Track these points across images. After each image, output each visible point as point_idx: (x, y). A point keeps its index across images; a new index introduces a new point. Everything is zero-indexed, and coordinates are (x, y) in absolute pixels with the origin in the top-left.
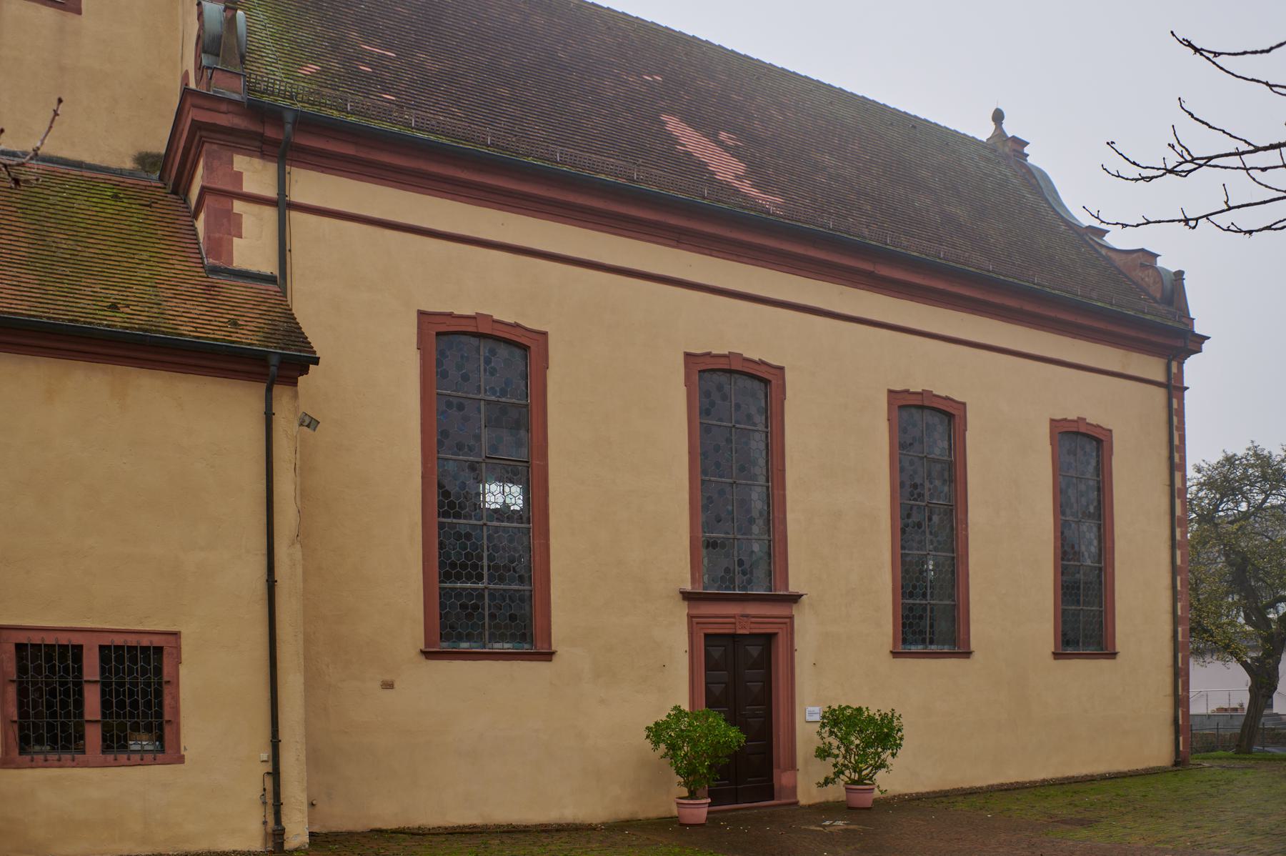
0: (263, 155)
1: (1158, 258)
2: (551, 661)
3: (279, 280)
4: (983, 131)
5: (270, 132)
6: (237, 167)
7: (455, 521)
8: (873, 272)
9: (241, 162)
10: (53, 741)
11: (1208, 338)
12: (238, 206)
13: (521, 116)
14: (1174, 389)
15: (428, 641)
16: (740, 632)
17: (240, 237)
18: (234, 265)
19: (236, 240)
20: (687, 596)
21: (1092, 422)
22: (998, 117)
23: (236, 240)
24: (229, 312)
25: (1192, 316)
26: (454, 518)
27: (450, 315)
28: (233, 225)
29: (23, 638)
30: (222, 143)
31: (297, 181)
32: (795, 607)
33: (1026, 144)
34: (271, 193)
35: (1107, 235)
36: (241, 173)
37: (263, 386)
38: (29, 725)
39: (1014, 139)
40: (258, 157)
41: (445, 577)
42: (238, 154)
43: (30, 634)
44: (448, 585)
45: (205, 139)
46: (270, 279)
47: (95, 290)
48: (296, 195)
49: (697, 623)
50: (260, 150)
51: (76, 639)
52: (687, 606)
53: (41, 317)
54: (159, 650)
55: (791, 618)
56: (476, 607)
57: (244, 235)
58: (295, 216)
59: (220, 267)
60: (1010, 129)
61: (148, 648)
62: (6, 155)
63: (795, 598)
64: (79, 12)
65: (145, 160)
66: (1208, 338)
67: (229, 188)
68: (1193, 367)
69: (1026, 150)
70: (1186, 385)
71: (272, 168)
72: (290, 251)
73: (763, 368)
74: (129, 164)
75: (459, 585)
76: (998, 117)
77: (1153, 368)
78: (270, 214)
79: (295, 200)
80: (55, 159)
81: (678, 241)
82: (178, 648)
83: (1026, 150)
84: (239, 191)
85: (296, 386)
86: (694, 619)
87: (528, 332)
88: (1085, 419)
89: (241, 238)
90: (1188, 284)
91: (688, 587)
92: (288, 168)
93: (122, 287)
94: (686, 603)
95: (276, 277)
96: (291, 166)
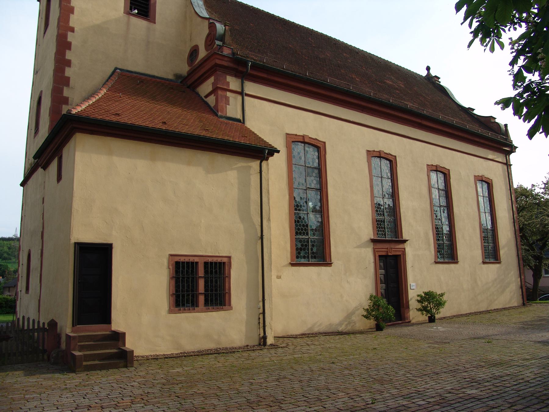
0: (236, 76)
1: (496, 119)
2: (331, 266)
3: (242, 121)
4: (424, 73)
5: (241, 69)
7: (299, 212)
8: (421, 123)
9: (229, 79)
11: (518, 147)
12: (229, 94)
14: (508, 165)
15: (292, 260)
16: (390, 254)
20: (373, 241)
21: (486, 177)
22: (428, 69)
25: (512, 140)
26: (299, 211)
27: (296, 135)
29: (207, 259)
31: (246, 86)
32: (405, 244)
33: (439, 78)
34: (239, 90)
35: (474, 110)
36: (229, 82)
37: (258, 162)
38: (213, 294)
39: (436, 76)
40: (234, 77)
41: (297, 233)
43: (180, 258)
44: (297, 237)
45: (217, 70)
46: (238, 120)
47: (132, 121)
48: (247, 91)
49: (377, 251)
51: (196, 259)
52: (373, 244)
53: (206, 136)
54: (177, 263)
55: (405, 249)
56: (306, 246)
58: (246, 98)
60: (433, 73)
61: (189, 262)
62: (130, 72)
63: (405, 241)
64: (155, 23)
65: (178, 76)
66: (518, 147)
67: (225, 87)
68: (512, 156)
69: (440, 80)
70: (511, 164)
71: (239, 81)
73: (390, 156)
74: (171, 77)
75: (301, 237)
76: (428, 69)
77: (500, 158)
78: (239, 98)
80: (183, 75)
81: (362, 111)
82: (230, 263)
83: (440, 80)
84: (228, 88)
86: (376, 250)
87: (314, 140)
88: (484, 176)
90: (509, 128)
91: (372, 238)
94: (372, 243)
96: (245, 80)
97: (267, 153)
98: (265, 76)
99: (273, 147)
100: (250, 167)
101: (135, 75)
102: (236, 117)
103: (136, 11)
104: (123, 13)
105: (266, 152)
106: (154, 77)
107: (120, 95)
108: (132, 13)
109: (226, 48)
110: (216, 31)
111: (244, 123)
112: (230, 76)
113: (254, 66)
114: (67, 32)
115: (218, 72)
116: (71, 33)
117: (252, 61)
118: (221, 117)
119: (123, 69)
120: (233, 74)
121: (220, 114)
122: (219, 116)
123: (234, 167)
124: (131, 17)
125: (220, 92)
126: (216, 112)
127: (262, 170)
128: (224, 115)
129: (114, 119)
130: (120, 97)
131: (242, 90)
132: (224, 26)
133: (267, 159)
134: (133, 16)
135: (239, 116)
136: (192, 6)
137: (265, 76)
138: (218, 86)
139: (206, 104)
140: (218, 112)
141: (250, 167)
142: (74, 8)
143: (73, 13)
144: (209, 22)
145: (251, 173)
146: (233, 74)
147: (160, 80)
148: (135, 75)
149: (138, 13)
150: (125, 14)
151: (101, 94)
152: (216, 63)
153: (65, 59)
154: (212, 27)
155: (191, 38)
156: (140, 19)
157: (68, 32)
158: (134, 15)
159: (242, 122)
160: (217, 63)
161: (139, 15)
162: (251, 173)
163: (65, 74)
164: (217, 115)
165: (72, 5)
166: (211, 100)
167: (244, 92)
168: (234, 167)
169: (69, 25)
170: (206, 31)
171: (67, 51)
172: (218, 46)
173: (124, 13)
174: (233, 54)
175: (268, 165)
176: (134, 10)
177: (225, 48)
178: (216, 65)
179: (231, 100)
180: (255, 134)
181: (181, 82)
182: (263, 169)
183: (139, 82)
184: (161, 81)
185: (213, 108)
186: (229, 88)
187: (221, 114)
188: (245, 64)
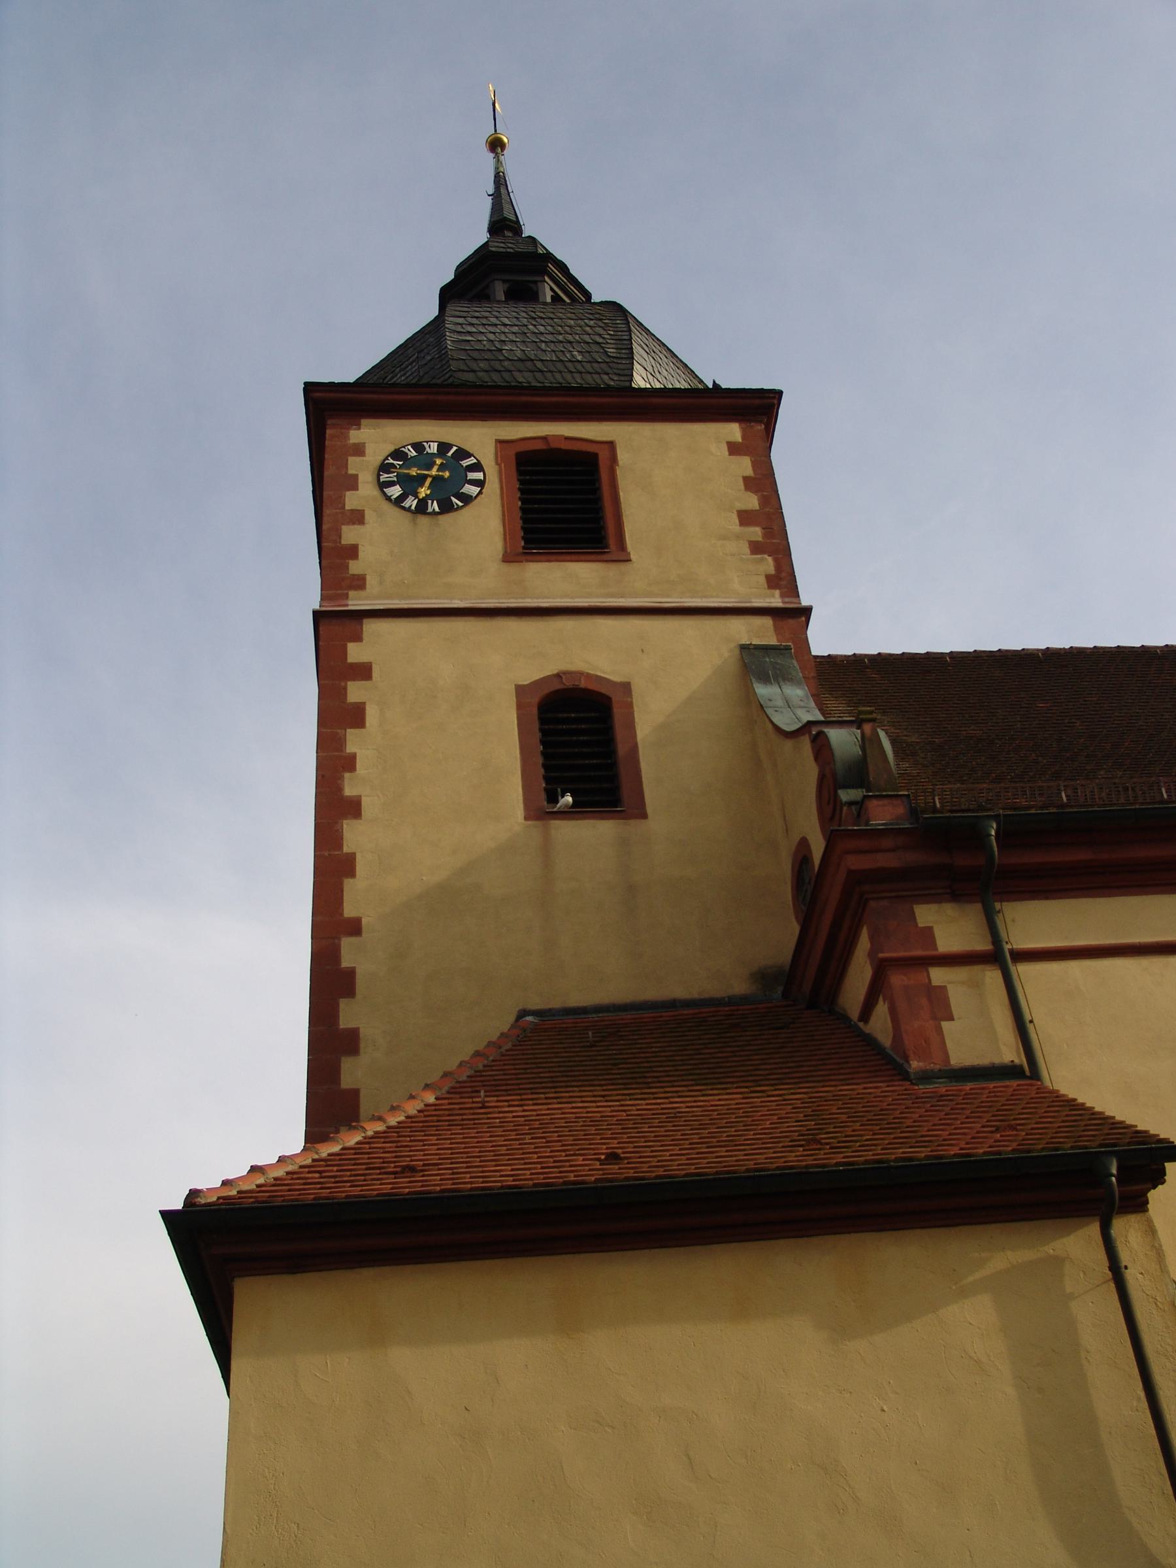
6: (922, 922)
9: (926, 915)
10: (341, 497)
12: (938, 975)
13: (441, 1123)
17: (951, 1018)
18: (952, 1062)
19: (945, 1025)
23: (945, 1025)
24: (579, 1054)
28: (939, 1006)
30: (893, 894)
34: (982, 945)
37: (1093, 1229)
42: (918, 903)
50: (948, 891)
57: (955, 1017)
58: (1025, 972)
59: (932, 1070)
64: (644, 816)
70: (805, 601)
71: (974, 911)
72: (1031, 1021)
74: (740, 987)
78: (992, 977)
79: (1019, 947)
85: (1146, 1210)
89: (953, 1020)
92: (997, 906)
93: (584, 1056)
95: (1021, 1067)
96: (1001, 901)
97: (1114, 1171)
98: (1082, 855)
99: (1142, 1137)
100: (1058, 1262)
101: (594, 1017)
102: (997, 1061)
103: (569, 799)
104: (523, 821)
105: (1108, 1169)
106: (672, 1004)
107: (480, 1100)
108: (555, 810)
109: (880, 803)
110: (833, 754)
111: (1035, 1074)
112: (927, 902)
113: (1009, 836)
114: (336, 941)
115: (872, 904)
116: (353, 939)
117: (999, 815)
118: (926, 1077)
119: (550, 1010)
120: (940, 891)
121: (915, 1065)
122: (912, 1076)
123: (970, 1279)
124: (556, 823)
125: (897, 980)
126: (901, 1061)
127: (1123, 1264)
128: (938, 1067)
129: (406, 1186)
130: (481, 1108)
131: (994, 943)
132: (858, 729)
133: (1138, 1205)
134: (559, 819)
135: (1009, 1053)
136: (764, 715)
137: (1082, 855)
138: (881, 955)
139: (870, 1041)
140: (908, 1062)
141: (1058, 1262)
142: (355, 859)
143: (351, 873)
144: (810, 736)
145: (1068, 1290)
146: (940, 891)
147: (691, 1012)
148: (594, 1017)
149: (575, 804)
150: (530, 822)
151: (404, 1112)
152: (850, 872)
153: (1147, 1193)
154: (821, 746)
155: (786, 824)
156: (585, 818)
157: (340, 939)
158: (565, 814)
159: (1028, 1073)
160: (853, 868)
161: (579, 810)
162: (1068, 1290)
163: (340, 1084)
164: (904, 1075)
165: (346, 849)
166: (880, 1025)
167: (1007, 947)
168: (970, 1279)
169: (342, 914)
170: (811, 772)
171: (343, 1004)
172: (853, 808)
173: (526, 818)
174: (914, 812)
175: (1151, 1230)
176: (563, 797)
177: (875, 802)
178: (856, 879)
179: (958, 997)
180: (1078, 1105)
181: (785, 995)
182: (1124, 1257)
183: (591, 1038)
184: (696, 1011)
185: (891, 1053)
186: (936, 948)
187: (920, 1064)
188: (973, 836)
